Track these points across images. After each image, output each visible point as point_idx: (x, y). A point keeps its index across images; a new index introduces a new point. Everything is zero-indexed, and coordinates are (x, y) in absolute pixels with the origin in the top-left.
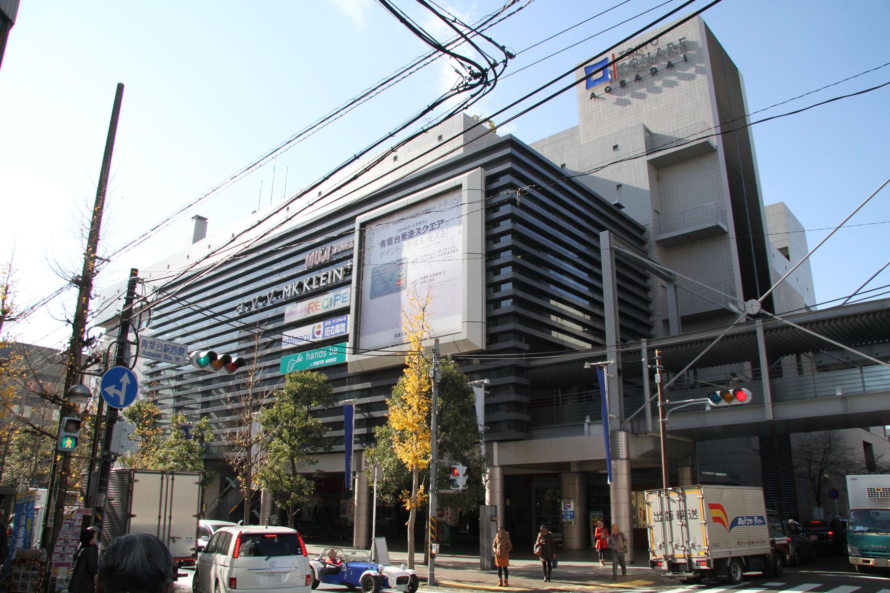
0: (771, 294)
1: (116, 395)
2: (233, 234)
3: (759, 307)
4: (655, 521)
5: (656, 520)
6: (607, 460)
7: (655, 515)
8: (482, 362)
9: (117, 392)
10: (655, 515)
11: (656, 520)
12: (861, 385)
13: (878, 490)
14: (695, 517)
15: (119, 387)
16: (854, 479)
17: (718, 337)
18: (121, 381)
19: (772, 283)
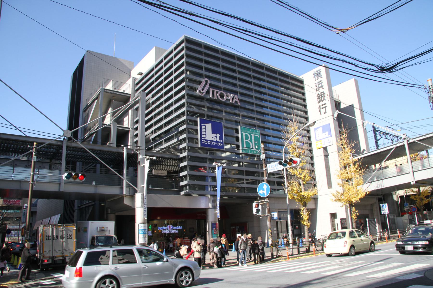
0: (78, 130)
1: (263, 193)
2: (339, 184)
3: (71, 135)
4: (47, 240)
5: (48, 239)
6: (117, 214)
7: (47, 237)
8: (423, 237)
9: (263, 192)
10: (47, 237)
11: (48, 239)
12: (15, 171)
13: (103, 228)
14: (70, 238)
15: (263, 190)
16: (92, 223)
17: (45, 143)
18: (263, 188)
19: (79, 126)
